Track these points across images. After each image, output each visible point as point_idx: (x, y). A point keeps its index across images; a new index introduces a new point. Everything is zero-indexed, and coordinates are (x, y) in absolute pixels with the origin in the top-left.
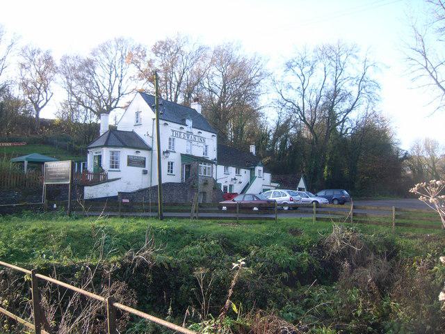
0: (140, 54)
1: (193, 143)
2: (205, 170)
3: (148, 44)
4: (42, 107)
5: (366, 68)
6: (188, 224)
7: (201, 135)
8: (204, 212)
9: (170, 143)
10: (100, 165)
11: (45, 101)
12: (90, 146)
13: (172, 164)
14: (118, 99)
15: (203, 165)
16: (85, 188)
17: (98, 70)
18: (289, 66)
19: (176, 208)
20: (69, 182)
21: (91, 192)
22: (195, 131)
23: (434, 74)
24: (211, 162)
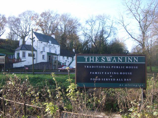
0: (36, 17)
1: (52, 49)
2: (55, 58)
3: (40, 13)
4: (1, 35)
5: (112, 23)
6: (41, 76)
7: (54, 46)
8: (47, 72)
9: (43, 49)
10: (19, 57)
11: (2, 33)
12: (16, 50)
13: (44, 55)
14: (29, 32)
15: (54, 56)
16: (14, 64)
17: (22, 22)
18: (87, 22)
19: (39, 71)
20: (4, 63)
21: (15, 65)
22: (52, 45)
23: (125, 28)
24: (58, 55)
